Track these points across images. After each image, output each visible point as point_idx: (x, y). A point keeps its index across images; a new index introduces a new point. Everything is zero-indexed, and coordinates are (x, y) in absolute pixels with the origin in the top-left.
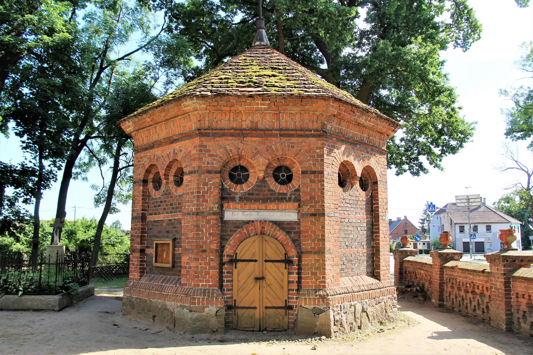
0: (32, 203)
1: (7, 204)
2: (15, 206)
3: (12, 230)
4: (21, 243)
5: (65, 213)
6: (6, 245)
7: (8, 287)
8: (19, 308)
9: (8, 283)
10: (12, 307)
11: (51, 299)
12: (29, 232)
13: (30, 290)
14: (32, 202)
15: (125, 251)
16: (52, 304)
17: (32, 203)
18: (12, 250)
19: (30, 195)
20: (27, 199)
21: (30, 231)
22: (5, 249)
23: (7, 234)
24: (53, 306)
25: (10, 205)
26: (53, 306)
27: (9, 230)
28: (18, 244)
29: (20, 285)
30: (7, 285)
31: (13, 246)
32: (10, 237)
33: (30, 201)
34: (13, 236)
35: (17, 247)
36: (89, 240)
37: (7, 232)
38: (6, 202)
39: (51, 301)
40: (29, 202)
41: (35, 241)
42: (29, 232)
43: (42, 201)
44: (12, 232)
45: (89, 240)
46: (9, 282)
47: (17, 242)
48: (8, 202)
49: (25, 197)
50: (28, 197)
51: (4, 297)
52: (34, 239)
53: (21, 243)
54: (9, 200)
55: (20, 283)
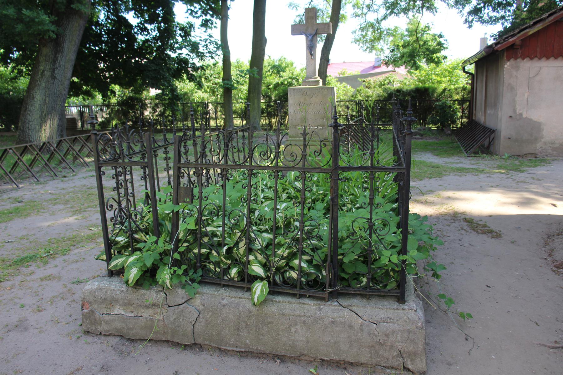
0: (215, 27)
1: (180, 35)
2: (191, 36)
3: (191, 72)
4: (203, 90)
5: (266, 40)
6: (186, 94)
7: (208, 256)
8: (261, 348)
9: (206, 240)
10: (232, 341)
11: (392, 327)
12: (211, 76)
13: (294, 275)
14: (214, 24)
15: (352, 96)
16: (400, 345)
17: (215, 27)
18: (194, 100)
19: (211, 13)
20: (207, 21)
21: (212, 75)
22: (185, 99)
23: (185, 78)
24: (400, 354)
25: (184, 36)
26: (400, 354)
27: (187, 73)
28: (199, 91)
29: (250, 250)
30: (201, 246)
31: (194, 94)
32: (190, 81)
33: (212, 24)
34: (193, 80)
35: (199, 95)
36: (286, 83)
37: (185, 75)
38: (179, 32)
39: (393, 332)
40: (209, 24)
41: (228, 84)
42: (211, 76)
43: (230, 23)
44: (191, 74)
45: (286, 83)
46: (206, 234)
47: (198, 89)
48: (181, 32)
49: (204, 17)
50: (208, 17)
51: (197, 302)
52: (226, 82)
53: (203, 90)
54: (182, 29)
55: (250, 242)
